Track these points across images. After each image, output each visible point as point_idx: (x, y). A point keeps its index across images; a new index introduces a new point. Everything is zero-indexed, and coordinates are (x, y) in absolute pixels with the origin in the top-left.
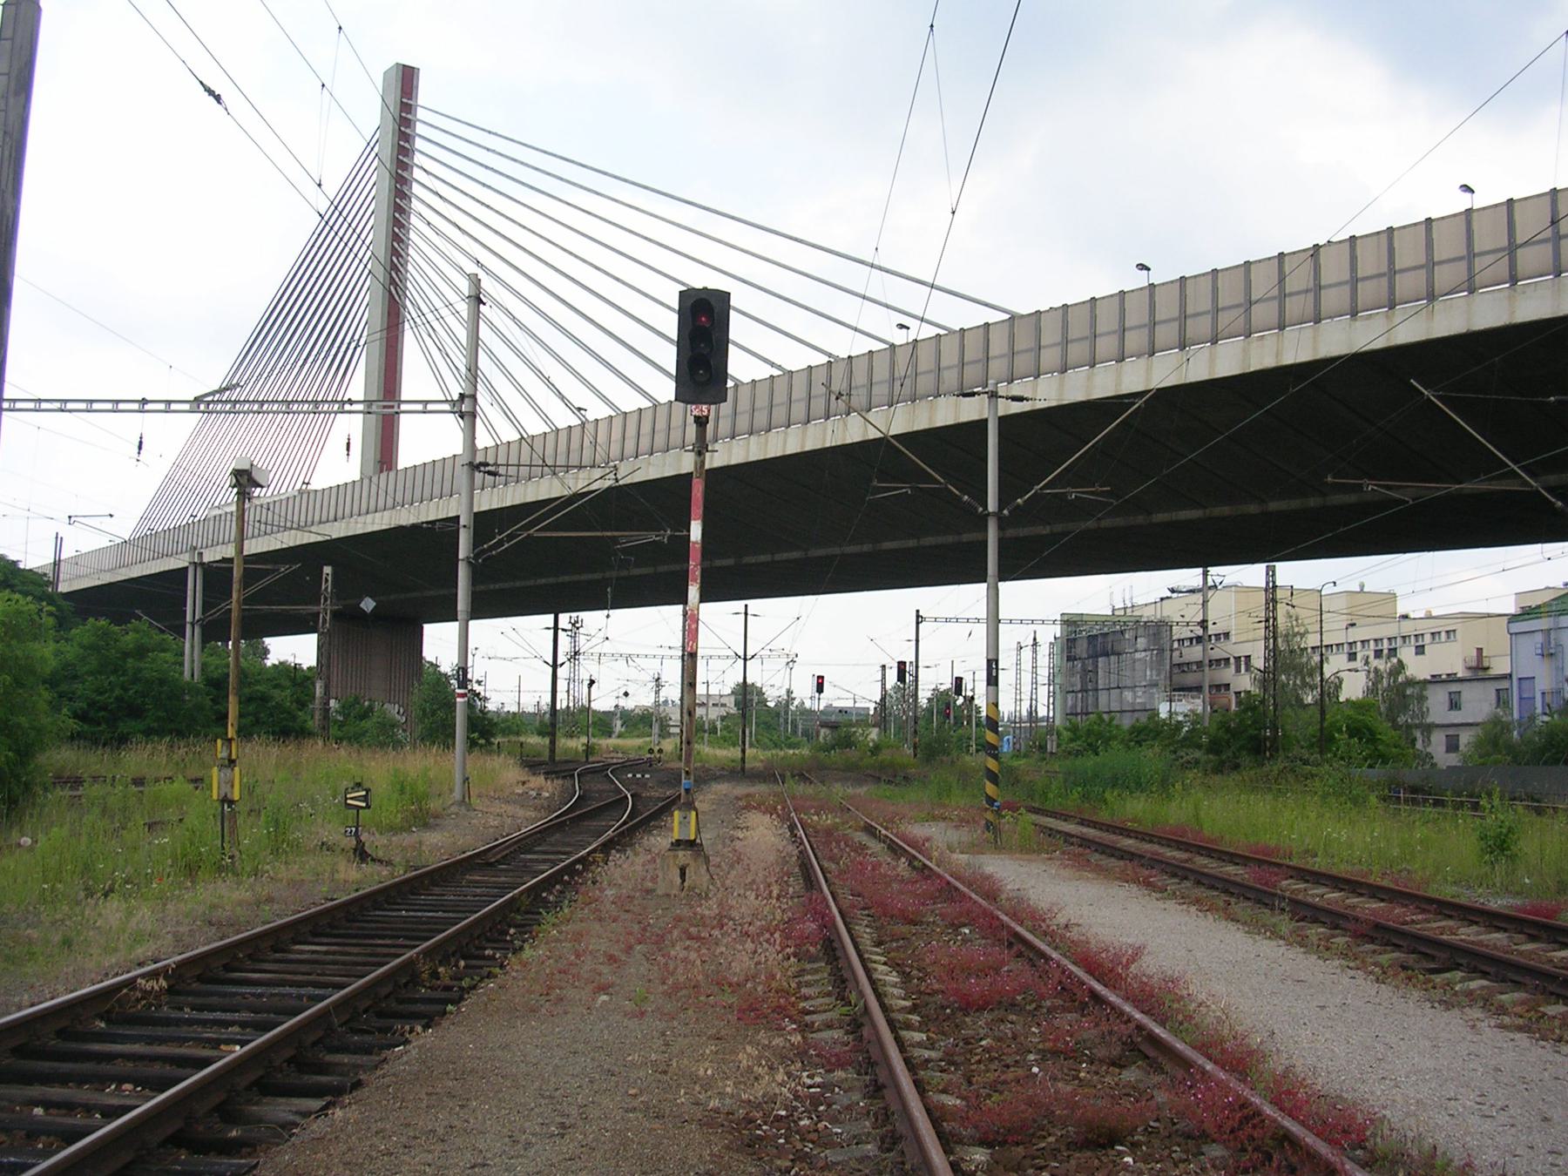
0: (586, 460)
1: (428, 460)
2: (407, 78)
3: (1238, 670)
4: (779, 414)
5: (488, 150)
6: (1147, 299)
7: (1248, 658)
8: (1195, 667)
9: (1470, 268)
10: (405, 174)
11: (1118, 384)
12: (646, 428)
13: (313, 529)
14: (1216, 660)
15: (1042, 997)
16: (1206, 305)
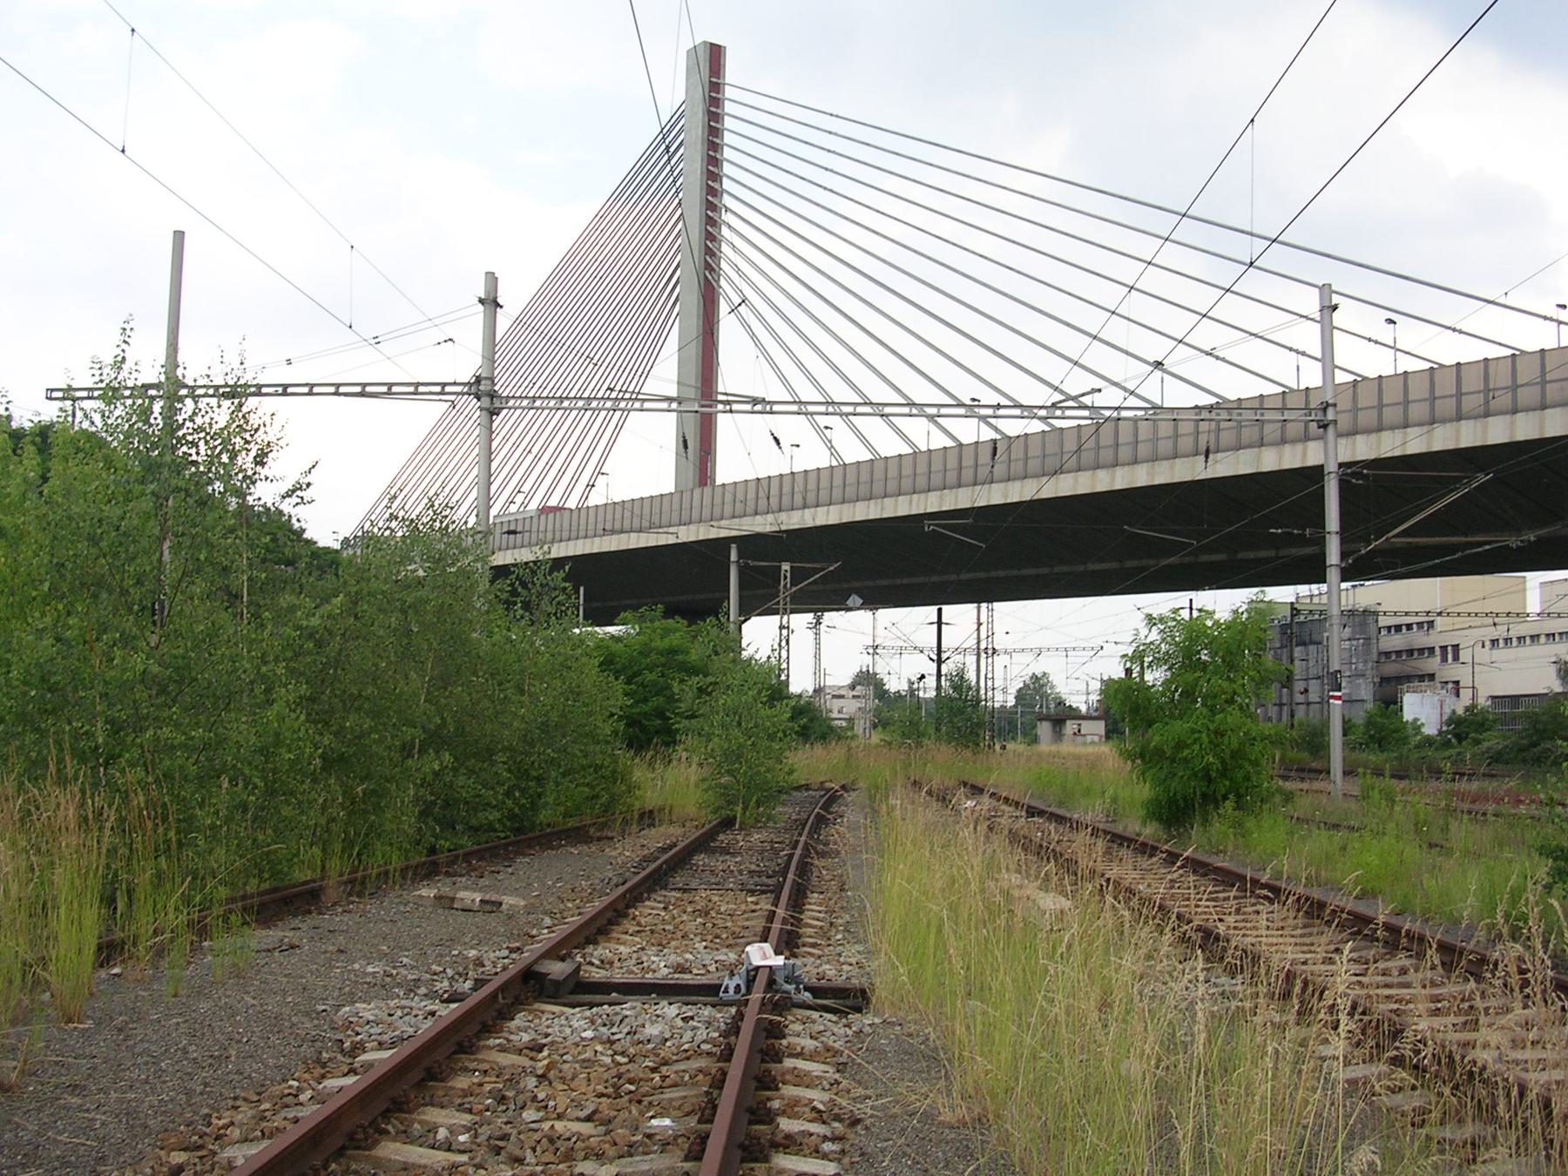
0: (627, 525)
1: (636, 496)
2: (715, 54)
3: (1444, 659)
4: (574, 534)
5: (826, 169)
6: (1538, 362)
7: (1456, 648)
8: (1394, 657)
9: (1175, 443)
10: (716, 186)
11: (1458, 440)
12: (786, 489)
13: (723, 523)
14: (1397, 652)
15: (401, 772)
16: (1038, 452)
